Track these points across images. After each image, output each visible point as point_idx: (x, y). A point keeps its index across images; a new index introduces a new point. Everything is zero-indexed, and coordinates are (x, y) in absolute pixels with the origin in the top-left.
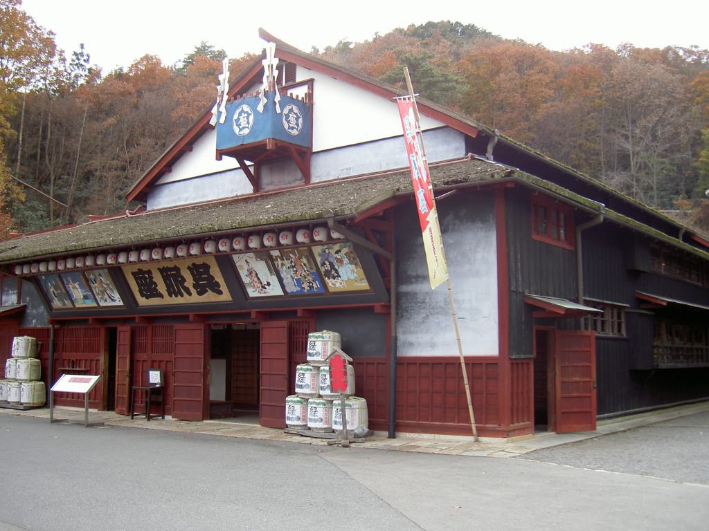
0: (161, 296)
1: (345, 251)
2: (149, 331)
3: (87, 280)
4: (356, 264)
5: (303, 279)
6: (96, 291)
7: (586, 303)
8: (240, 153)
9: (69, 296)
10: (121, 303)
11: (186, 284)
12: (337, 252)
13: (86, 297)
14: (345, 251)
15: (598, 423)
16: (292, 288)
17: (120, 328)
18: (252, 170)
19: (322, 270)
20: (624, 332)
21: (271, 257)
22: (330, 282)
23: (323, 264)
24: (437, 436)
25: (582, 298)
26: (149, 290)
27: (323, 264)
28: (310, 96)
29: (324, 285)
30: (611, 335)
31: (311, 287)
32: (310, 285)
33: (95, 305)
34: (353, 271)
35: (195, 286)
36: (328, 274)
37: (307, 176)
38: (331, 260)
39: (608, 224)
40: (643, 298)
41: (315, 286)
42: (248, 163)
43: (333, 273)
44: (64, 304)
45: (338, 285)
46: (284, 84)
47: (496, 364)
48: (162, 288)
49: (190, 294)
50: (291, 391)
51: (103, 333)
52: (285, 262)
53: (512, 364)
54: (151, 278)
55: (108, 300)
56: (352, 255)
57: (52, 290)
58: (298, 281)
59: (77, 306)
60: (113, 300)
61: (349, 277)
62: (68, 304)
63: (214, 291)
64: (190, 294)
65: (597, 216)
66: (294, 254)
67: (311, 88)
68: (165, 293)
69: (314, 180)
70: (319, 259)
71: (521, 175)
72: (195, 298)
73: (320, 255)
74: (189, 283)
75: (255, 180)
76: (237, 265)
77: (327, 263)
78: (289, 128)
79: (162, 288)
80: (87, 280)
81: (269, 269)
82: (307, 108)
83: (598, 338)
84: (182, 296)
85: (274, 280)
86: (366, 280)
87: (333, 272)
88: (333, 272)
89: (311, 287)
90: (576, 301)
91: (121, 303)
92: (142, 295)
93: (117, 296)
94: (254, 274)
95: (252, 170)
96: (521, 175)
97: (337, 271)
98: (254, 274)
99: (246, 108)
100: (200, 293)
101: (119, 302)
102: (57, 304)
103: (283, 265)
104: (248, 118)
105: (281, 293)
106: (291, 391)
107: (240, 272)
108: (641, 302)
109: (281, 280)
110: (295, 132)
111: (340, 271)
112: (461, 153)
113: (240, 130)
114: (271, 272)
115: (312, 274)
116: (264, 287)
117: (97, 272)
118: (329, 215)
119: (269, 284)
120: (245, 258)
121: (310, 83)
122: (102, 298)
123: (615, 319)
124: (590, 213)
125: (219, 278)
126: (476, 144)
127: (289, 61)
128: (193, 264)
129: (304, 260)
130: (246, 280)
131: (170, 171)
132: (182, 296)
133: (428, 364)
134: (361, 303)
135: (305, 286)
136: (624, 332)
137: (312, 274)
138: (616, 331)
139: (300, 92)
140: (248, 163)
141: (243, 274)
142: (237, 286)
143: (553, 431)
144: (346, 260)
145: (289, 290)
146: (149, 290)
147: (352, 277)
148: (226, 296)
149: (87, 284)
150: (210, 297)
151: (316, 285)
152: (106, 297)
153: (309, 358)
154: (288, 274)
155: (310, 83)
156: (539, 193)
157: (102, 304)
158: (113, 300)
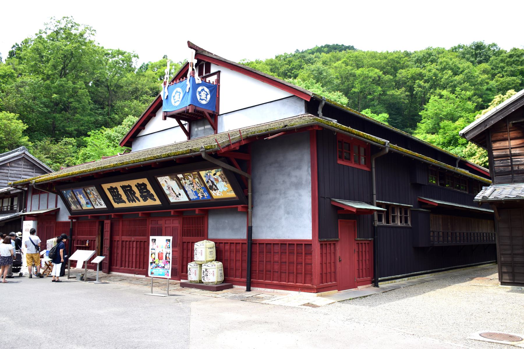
0: (125, 202)
1: (218, 174)
2: (121, 223)
3: (86, 193)
4: (226, 182)
5: (198, 191)
6: (92, 199)
7: (379, 205)
8: (178, 116)
9: (79, 202)
10: (105, 207)
11: (136, 195)
12: (215, 174)
13: (87, 203)
14: (218, 174)
15: (379, 283)
16: (193, 197)
17: (106, 221)
18: (186, 127)
19: (208, 185)
20: (409, 223)
21: (178, 178)
22: (213, 193)
23: (208, 182)
24: (275, 290)
25: (376, 201)
26: (119, 200)
28: (218, 81)
30: (399, 224)
31: (203, 196)
32: (202, 195)
33: (92, 208)
34: (225, 186)
35: (141, 196)
37: (215, 128)
38: (212, 179)
39: (393, 154)
40: (422, 201)
41: (205, 195)
42: (183, 122)
43: (214, 187)
44: (77, 207)
45: (218, 194)
46: (204, 75)
47: (311, 244)
48: (124, 197)
49: (139, 201)
50: (192, 260)
51: (97, 224)
52: (187, 181)
53: (321, 245)
54: (118, 192)
55: (99, 205)
56: (223, 176)
57: (70, 199)
58: (195, 192)
59: (84, 208)
60: (101, 205)
61: (224, 190)
62: (79, 208)
63: (151, 199)
64: (139, 201)
65: (384, 149)
66: (191, 176)
68: (126, 201)
69: (219, 131)
70: (205, 179)
71: (322, 119)
73: (205, 177)
74: (138, 194)
75: (189, 134)
76: (161, 183)
77: (210, 181)
78: (201, 99)
79: (124, 197)
80: (86, 193)
81: (179, 185)
82: (215, 90)
84: (135, 202)
85: (182, 192)
86: (233, 192)
87: (214, 187)
88: (214, 187)
89: (203, 196)
90: (372, 204)
91: (105, 207)
92: (115, 202)
93: (102, 202)
94: (171, 189)
95: (186, 127)
96: (322, 119)
97: (216, 186)
98: (171, 189)
99: (179, 89)
100: (145, 200)
101: (104, 206)
102: (73, 207)
103: (185, 183)
104: (179, 95)
105: (187, 200)
106: (192, 260)
107: (163, 187)
108: (422, 204)
109: (186, 192)
110: (204, 102)
111: (217, 186)
112: (303, 112)
113: (175, 102)
114: (180, 188)
115: (203, 188)
116: (177, 196)
118: (202, 150)
119: (180, 194)
120: (165, 179)
121: (218, 73)
122: (95, 204)
123: (403, 215)
124: (378, 147)
125: (152, 192)
126: (313, 104)
127: (207, 61)
128: (138, 184)
129: (197, 180)
130: (167, 192)
131: (144, 129)
132: (135, 202)
133: (271, 244)
134: (226, 208)
135: (200, 195)
136: (409, 223)
137: (203, 188)
138: (403, 222)
139: (212, 79)
141: (165, 188)
142: (162, 196)
144: (220, 179)
145: (191, 198)
146: (119, 200)
147: (225, 190)
148: (158, 202)
150: (149, 202)
151: (206, 195)
152: (97, 203)
154: (189, 188)
155: (218, 73)
156: (337, 132)
157: (96, 207)
158: (101, 205)
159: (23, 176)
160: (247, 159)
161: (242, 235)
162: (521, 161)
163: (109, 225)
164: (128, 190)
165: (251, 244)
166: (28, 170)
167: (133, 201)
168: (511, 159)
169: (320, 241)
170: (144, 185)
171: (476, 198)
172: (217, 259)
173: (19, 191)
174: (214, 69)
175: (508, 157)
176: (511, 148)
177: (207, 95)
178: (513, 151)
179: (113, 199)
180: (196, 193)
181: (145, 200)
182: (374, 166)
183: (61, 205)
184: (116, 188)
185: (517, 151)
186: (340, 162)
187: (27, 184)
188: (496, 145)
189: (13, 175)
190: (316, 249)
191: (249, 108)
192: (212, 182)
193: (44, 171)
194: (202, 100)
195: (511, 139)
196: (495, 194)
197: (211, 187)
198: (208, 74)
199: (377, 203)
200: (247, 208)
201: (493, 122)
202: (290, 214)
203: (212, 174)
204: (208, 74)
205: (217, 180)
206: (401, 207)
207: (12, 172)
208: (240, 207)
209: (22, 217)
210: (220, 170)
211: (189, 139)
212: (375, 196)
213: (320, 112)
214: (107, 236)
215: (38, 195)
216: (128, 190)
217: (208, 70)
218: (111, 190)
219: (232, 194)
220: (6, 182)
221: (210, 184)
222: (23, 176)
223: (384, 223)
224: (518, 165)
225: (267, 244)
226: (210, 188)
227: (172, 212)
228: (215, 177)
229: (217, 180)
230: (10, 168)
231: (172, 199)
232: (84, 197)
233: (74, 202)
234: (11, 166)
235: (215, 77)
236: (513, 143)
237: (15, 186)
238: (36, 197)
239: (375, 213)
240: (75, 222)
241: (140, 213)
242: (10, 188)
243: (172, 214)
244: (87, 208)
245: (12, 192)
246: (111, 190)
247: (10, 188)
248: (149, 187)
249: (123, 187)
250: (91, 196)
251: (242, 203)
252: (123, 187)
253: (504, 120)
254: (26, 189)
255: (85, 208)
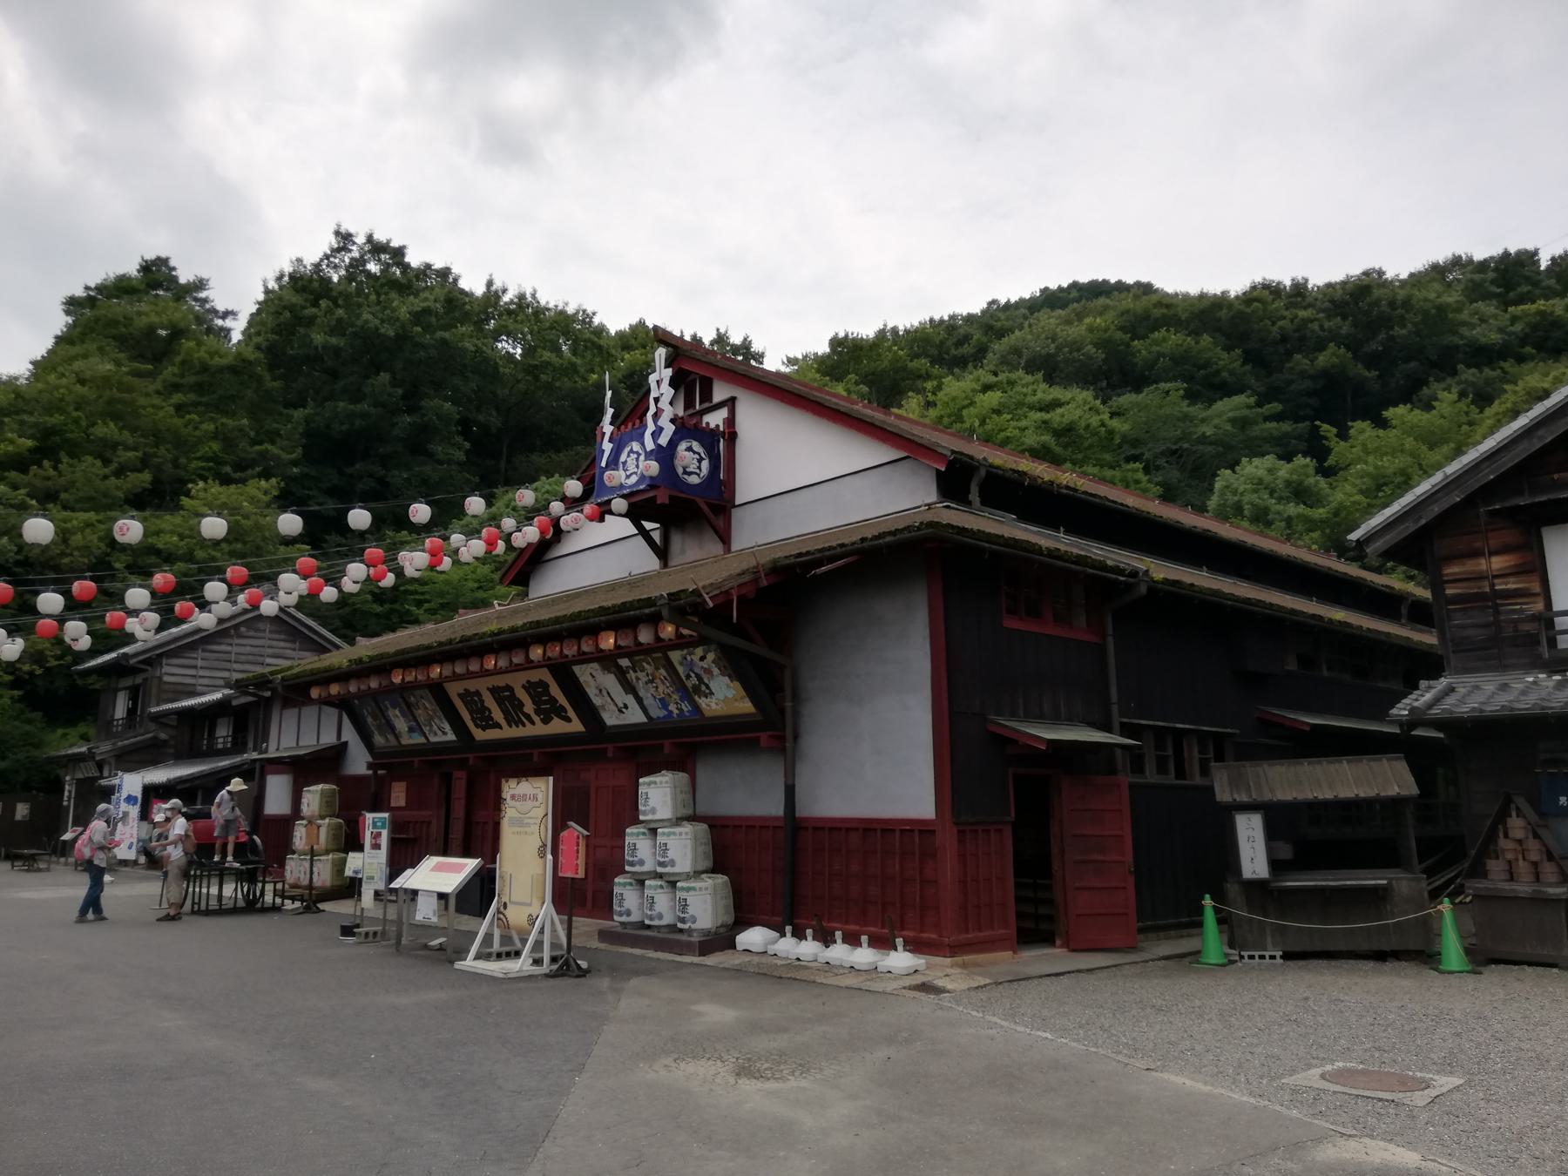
0: (498, 726)
1: (711, 656)
3: (409, 705)
6: (422, 720)
7: (1126, 730)
9: (393, 729)
11: (526, 710)
12: (702, 659)
13: (411, 730)
16: (656, 712)
18: (656, 536)
19: (689, 684)
22: (703, 702)
23: (688, 677)
25: (1116, 720)
26: (487, 722)
27: (688, 677)
28: (731, 421)
29: (697, 708)
33: (422, 740)
35: (537, 712)
36: (697, 689)
37: (725, 538)
42: (648, 525)
43: (702, 689)
48: (498, 715)
52: (640, 674)
58: (662, 700)
59: (404, 742)
60: (445, 733)
61: (725, 697)
62: (393, 742)
67: (732, 413)
68: (503, 722)
70: (680, 669)
72: (538, 729)
74: (529, 707)
75: (662, 552)
78: (685, 472)
79: (498, 715)
80: (409, 705)
83: (1132, 786)
85: (630, 700)
90: (1107, 728)
92: (477, 726)
93: (447, 727)
95: (656, 536)
97: (708, 687)
100: (546, 721)
101: (451, 737)
102: (378, 740)
105: (643, 719)
109: (639, 700)
110: (694, 480)
112: (932, 496)
117: (418, 692)
119: (626, 707)
125: (562, 700)
126: (956, 479)
129: (663, 671)
130: (597, 701)
135: (672, 707)
139: (715, 419)
140: (648, 525)
141: (591, 692)
143: (1061, 946)
144: (716, 671)
146: (487, 722)
148: (576, 726)
149: (409, 711)
150: (557, 727)
151: (686, 707)
153: (641, 818)
157: (433, 739)
158: (445, 733)
159: (268, 660)
160: (781, 616)
161: (770, 805)
162: (1522, 611)
163: (464, 782)
164: (505, 697)
165: (796, 833)
166: (282, 644)
167: (519, 723)
168: (1496, 606)
169: (956, 824)
170: (544, 685)
171: (1394, 711)
172: (715, 870)
173: (250, 699)
174: (720, 393)
175: (1458, 599)
176: (1495, 577)
177: (700, 460)
178: (1500, 586)
179: (473, 720)
180: (664, 704)
181: (546, 721)
182: (1110, 630)
183: (349, 734)
184: (478, 693)
185: (1512, 585)
186: (1011, 623)
187: (262, 682)
188: (1452, 570)
189: (243, 658)
190: (947, 841)
191: (805, 482)
192: (697, 676)
193: (321, 648)
194: (690, 474)
195: (1491, 554)
196: (1503, 699)
197: (697, 689)
198: (707, 405)
199: (1122, 725)
200: (783, 738)
201: (1436, 509)
202: (879, 753)
203: (696, 658)
204: (707, 405)
205: (708, 671)
206: (1202, 737)
207: (242, 650)
208: (764, 737)
209: (258, 765)
210: (713, 647)
211: (665, 564)
212: (1115, 708)
213: (974, 496)
214: (459, 810)
215: (296, 710)
216: (505, 697)
217: (707, 395)
218: (466, 696)
219: (746, 706)
220: (226, 674)
221: (694, 680)
222: (268, 660)
223: (1171, 779)
224: (1516, 622)
225: (831, 829)
226: (691, 691)
227: (610, 747)
228: (704, 664)
229: (708, 671)
230: (237, 641)
231: (611, 719)
232: (404, 715)
233: (379, 728)
234: (240, 636)
235: (723, 413)
236: (1498, 563)
237: (240, 686)
238: (290, 715)
239: (1118, 752)
240: (382, 777)
241: (536, 752)
242: (227, 691)
243: (610, 754)
244: (411, 742)
245: (234, 703)
246: (466, 696)
247: (227, 691)
248: (555, 691)
249: (494, 691)
250: (419, 712)
251: (772, 729)
252: (494, 691)
253: (1471, 500)
254: (268, 694)
255: (406, 741)
